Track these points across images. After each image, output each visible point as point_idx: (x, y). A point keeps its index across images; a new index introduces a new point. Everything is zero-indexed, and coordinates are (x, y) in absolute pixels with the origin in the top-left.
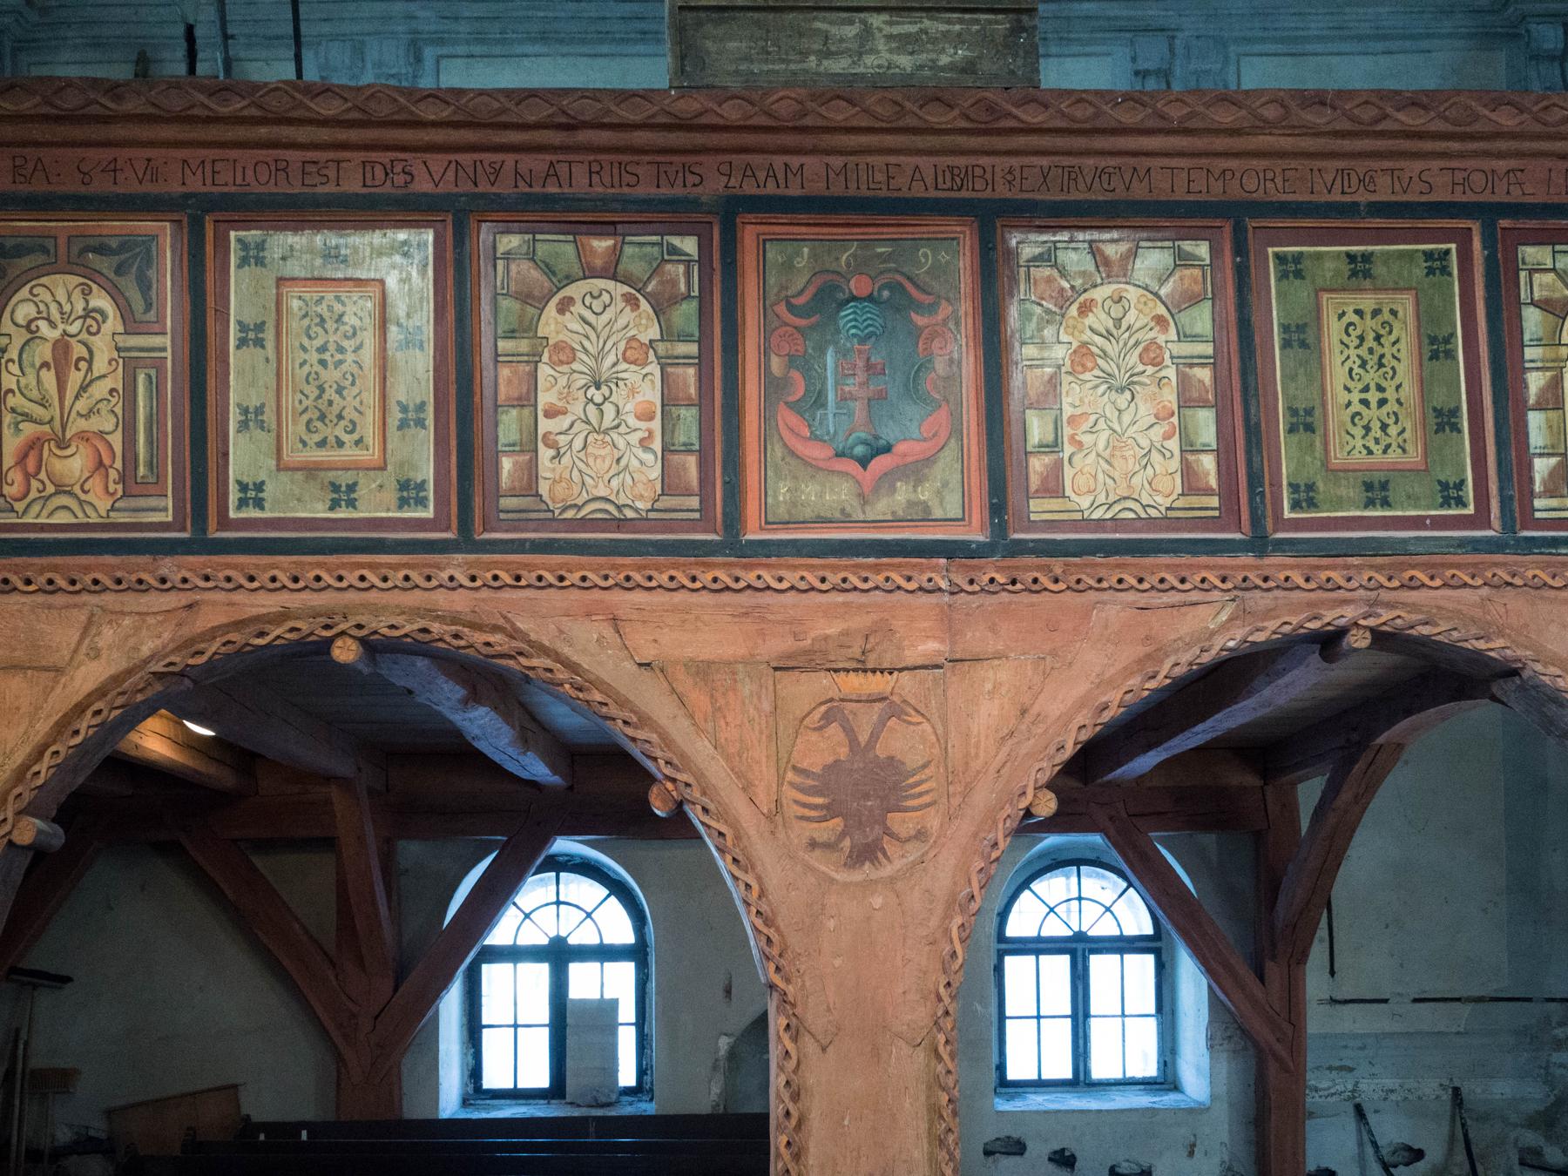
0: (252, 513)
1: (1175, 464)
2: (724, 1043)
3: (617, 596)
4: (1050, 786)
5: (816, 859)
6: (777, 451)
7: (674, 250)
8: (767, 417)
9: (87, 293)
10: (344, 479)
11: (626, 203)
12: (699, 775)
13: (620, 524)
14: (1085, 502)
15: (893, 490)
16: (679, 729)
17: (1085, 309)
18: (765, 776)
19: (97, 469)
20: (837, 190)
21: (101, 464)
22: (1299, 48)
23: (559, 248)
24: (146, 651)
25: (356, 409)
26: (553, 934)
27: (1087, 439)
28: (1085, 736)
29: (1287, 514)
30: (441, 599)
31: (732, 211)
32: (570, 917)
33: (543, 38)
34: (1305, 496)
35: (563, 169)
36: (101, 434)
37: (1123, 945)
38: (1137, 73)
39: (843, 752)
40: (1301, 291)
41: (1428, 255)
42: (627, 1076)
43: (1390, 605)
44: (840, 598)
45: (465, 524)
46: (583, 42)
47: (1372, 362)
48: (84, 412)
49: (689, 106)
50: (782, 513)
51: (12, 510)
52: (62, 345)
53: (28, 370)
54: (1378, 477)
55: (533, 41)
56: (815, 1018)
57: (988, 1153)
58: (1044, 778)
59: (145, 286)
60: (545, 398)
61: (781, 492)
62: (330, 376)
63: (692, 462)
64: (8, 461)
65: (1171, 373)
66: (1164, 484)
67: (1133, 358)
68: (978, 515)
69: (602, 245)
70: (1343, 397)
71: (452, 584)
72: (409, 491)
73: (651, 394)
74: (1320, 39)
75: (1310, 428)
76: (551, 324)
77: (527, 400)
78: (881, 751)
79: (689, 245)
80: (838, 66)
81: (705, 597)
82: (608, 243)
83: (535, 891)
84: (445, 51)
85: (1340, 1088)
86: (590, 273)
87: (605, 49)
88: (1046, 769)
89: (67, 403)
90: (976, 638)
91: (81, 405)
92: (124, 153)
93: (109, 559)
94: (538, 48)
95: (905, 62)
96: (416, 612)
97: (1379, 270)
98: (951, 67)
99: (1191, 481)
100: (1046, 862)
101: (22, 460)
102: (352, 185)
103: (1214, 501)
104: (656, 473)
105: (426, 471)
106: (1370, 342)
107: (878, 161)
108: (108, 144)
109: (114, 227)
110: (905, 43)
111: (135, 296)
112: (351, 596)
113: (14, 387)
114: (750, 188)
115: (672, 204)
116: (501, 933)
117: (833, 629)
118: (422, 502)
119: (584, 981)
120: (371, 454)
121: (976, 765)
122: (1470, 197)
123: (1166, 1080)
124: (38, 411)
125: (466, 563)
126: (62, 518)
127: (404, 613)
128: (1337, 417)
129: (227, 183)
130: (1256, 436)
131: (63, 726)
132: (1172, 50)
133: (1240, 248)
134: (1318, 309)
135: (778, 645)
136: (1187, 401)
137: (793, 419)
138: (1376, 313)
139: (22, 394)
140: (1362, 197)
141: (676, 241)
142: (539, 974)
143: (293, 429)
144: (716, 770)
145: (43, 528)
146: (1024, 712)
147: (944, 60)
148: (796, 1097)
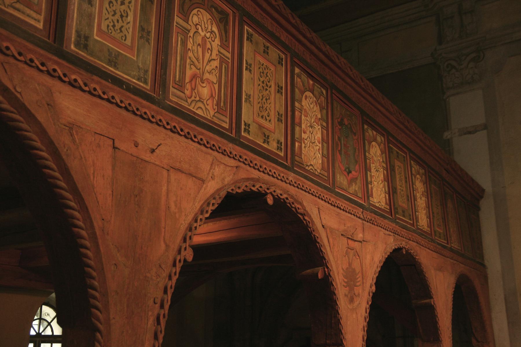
19: (211, 97)
25: (126, 29)
48: (209, 71)
51: (187, 102)
53: (195, 44)
89: (205, 64)
106: (118, 16)
113: (191, 48)
125: (294, 177)
127: (281, 190)
139: (193, 53)
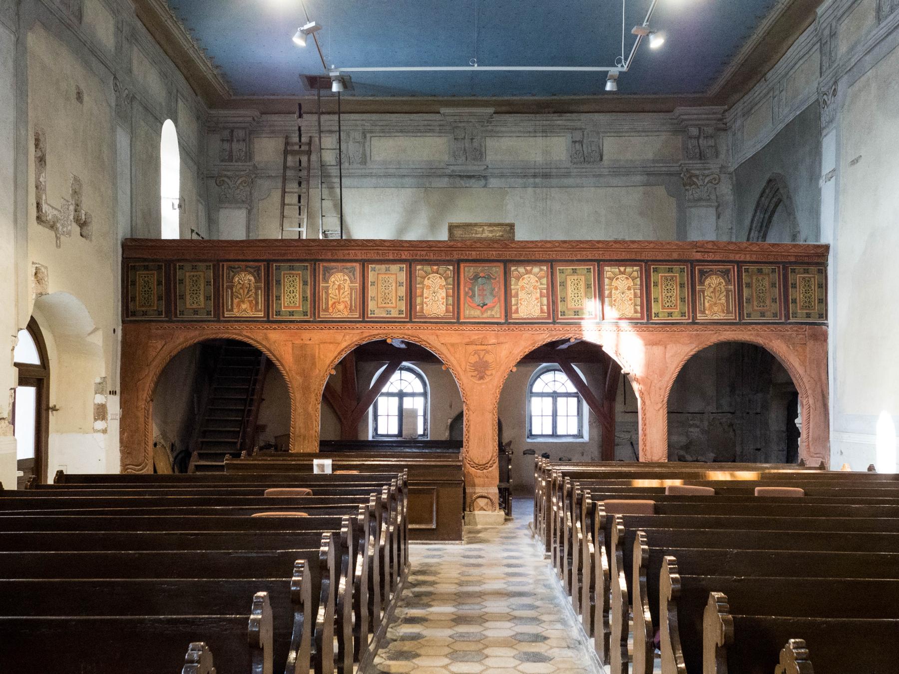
0: (373, 316)
1: (539, 308)
2: (450, 421)
3: (438, 331)
4: (515, 366)
5: (472, 379)
6: (466, 305)
7: (448, 269)
8: (465, 299)
9: (344, 276)
10: (389, 309)
11: (440, 260)
12: (452, 364)
13: (438, 318)
14: (522, 315)
15: (487, 312)
16: (448, 355)
17: (523, 279)
18: (463, 364)
20: (478, 258)
21: (346, 307)
22: (621, 134)
23: (428, 268)
24: (354, 340)
26: (399, 389)
27: (523, 303)
28: (522, 357)
29: (560, 317)
30: (406, 331)
31: (459, 262)
32: (404, 384)
33: (401, 131)
34: (563, 313)
35: (428, 254)
36: (346, 301)
37: (568, 395)
38: (573, 142)
39: (478, 360)
40: (563, 276)
41: (587, 269)
42: (420, 431)
43: (578, 334)
44: (477, 332)
45: (411, 318)
46: (413, 132)
47: (576, 289)
49: (452, 243)
50: (467, 316)
52: (339, 286)
54: (577, 310)
55: (398, 132)
56: (472, 407)
57: (524, 454)
58: (514, 365)
59: (354, 275)
60: (425, 295)
61: (467, 312)
62: (387, 291)
63: (451, 307)
64: (330, 306)
65: (539, 291)
66: (537, 311)
67: (532, 288)
68: (503, 316)
69: (435, 267)
70: (571, 295)
71: (408, 329)
72: (401, 312)
73: (444, 295)
74: (626, 132)
75: (564, 301)
76: (426, 282)
77: (422, 295)
78: (484, 360)
79: (451, 268)
80: (479, 236)
81: (453, 332)
82: (437, 267)
83: (396, 376)
84: (373, 135)
85: (626, 437)
86: (433, 272)
87: (419, 134)
88: (514, 363)
90: (502, 339)
91: (343, 296)
92: (351, 251)
93: (349, 324)
94: (399, 134)
95: (490, 235)
96: (402, 334)
97: (578, 271)
98: (499, 236)
99: (542, 311)
100: (545, 370)
101: (332, 306)
102: (391, 257)
103: (546, 315)
104: (445, 309)
105: (404, 309)
106: (576, 285)
107: (486, 252)
108: (347, 250)
109: (349, 265)
110: (491, 232)
111: (352, 277)
112: (391, 331)
114: (462, 258)
115: (448, 261)
116: (385, 390)
117: (476, 337)
118: (403, 314)
119: (408, 403)
120: (394, 305)
121: (502, 362)
122: (595, 258)
123: (580, 435)
124: (335, 297)
126: (339, 316)
128: (569, 299)
129: (369, 257)
130: (554, 303)
131: (339, 353)
132: (583, 135)
133: (552, 268)
134: (566, 278)
135: (467, 340)
136: (541, 296)
137: (470, 299)
138: (577, 279)
140: (575, 258)
141: (449, 267)
142: (396, 400)
143: (380, 300)
144: (455, 363)
145: (335, 318)
146: (510, 353)
147: (498, 235)
148: (468, 421)
